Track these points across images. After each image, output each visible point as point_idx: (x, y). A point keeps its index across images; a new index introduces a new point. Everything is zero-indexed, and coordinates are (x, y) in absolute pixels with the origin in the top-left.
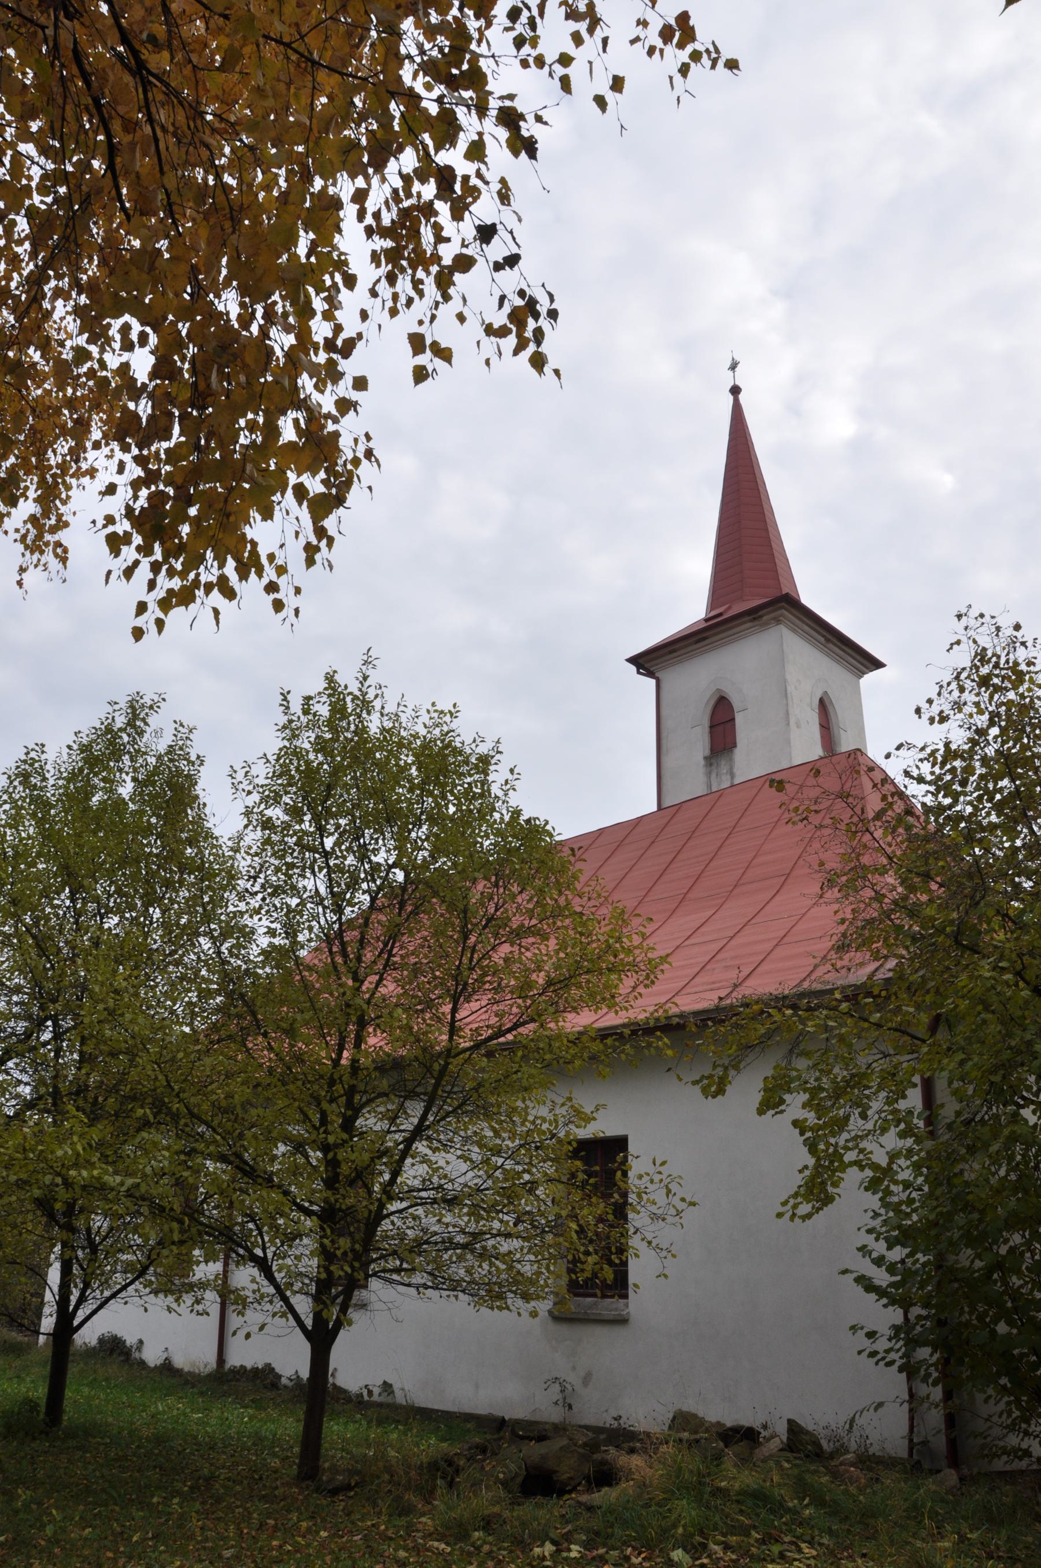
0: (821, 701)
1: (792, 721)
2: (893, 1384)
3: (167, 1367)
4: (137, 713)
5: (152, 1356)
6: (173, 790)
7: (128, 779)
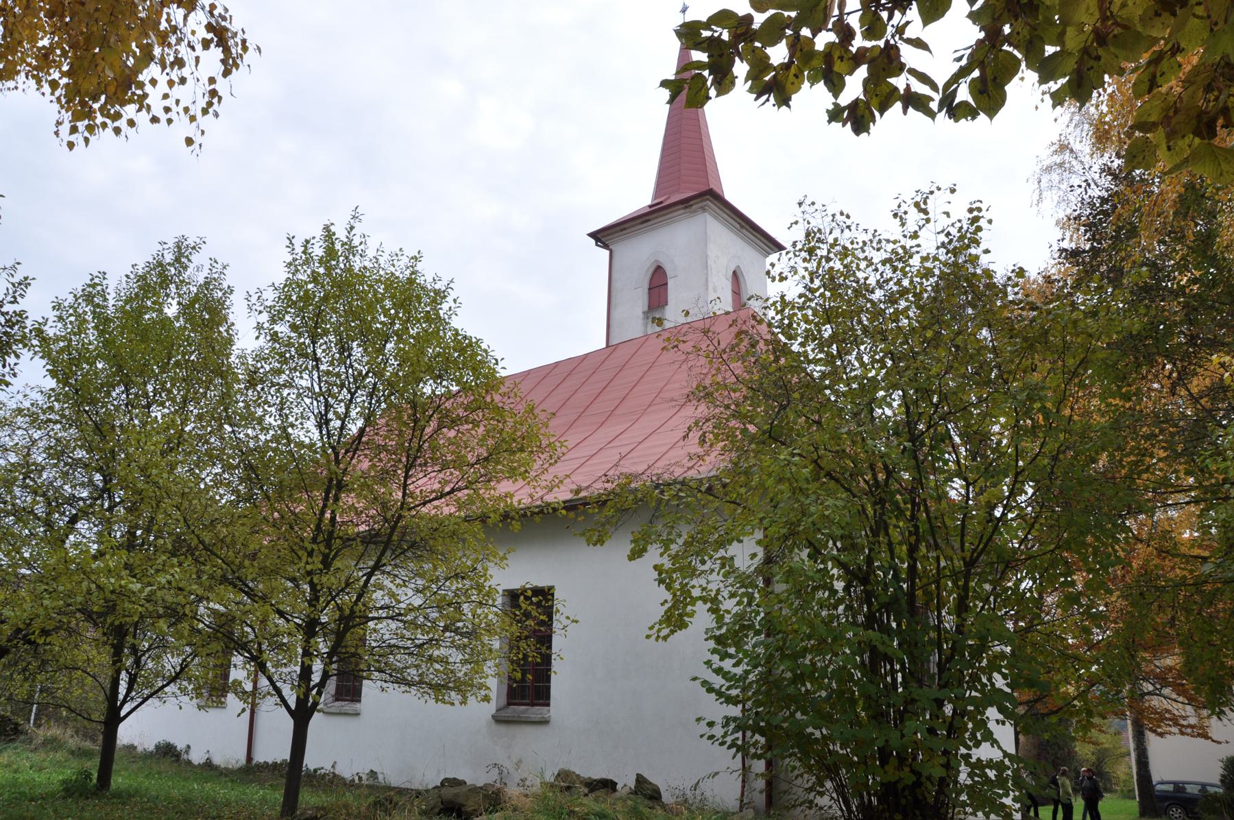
0: (735, 273)
1: (710, 286)
2: (728, 760)
3: (208, 765)
4: (182, 253)
5: (197, 757)
6: (208, 311)
7: (174, 302)
